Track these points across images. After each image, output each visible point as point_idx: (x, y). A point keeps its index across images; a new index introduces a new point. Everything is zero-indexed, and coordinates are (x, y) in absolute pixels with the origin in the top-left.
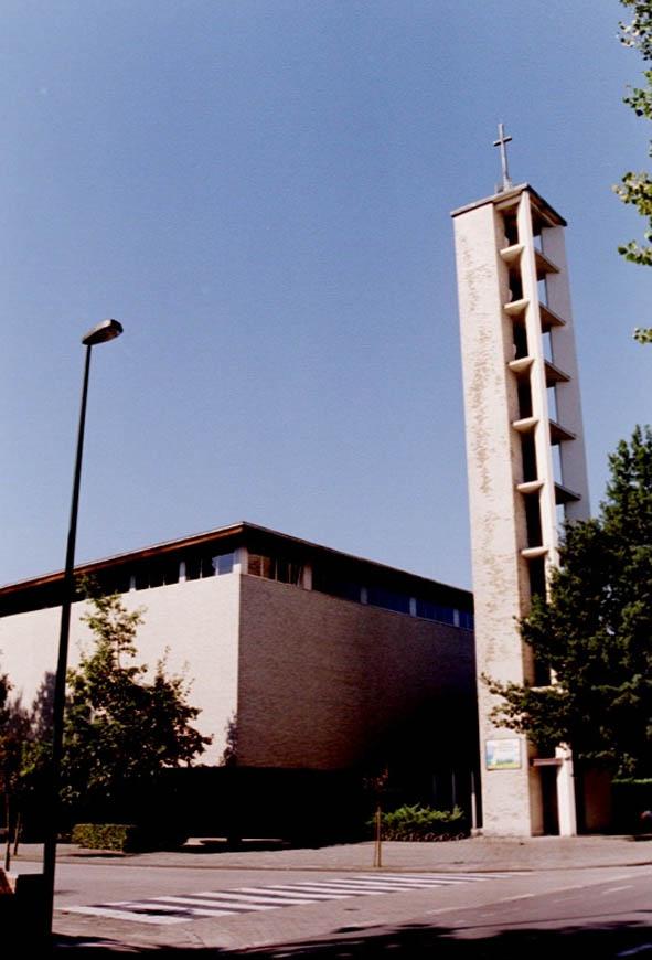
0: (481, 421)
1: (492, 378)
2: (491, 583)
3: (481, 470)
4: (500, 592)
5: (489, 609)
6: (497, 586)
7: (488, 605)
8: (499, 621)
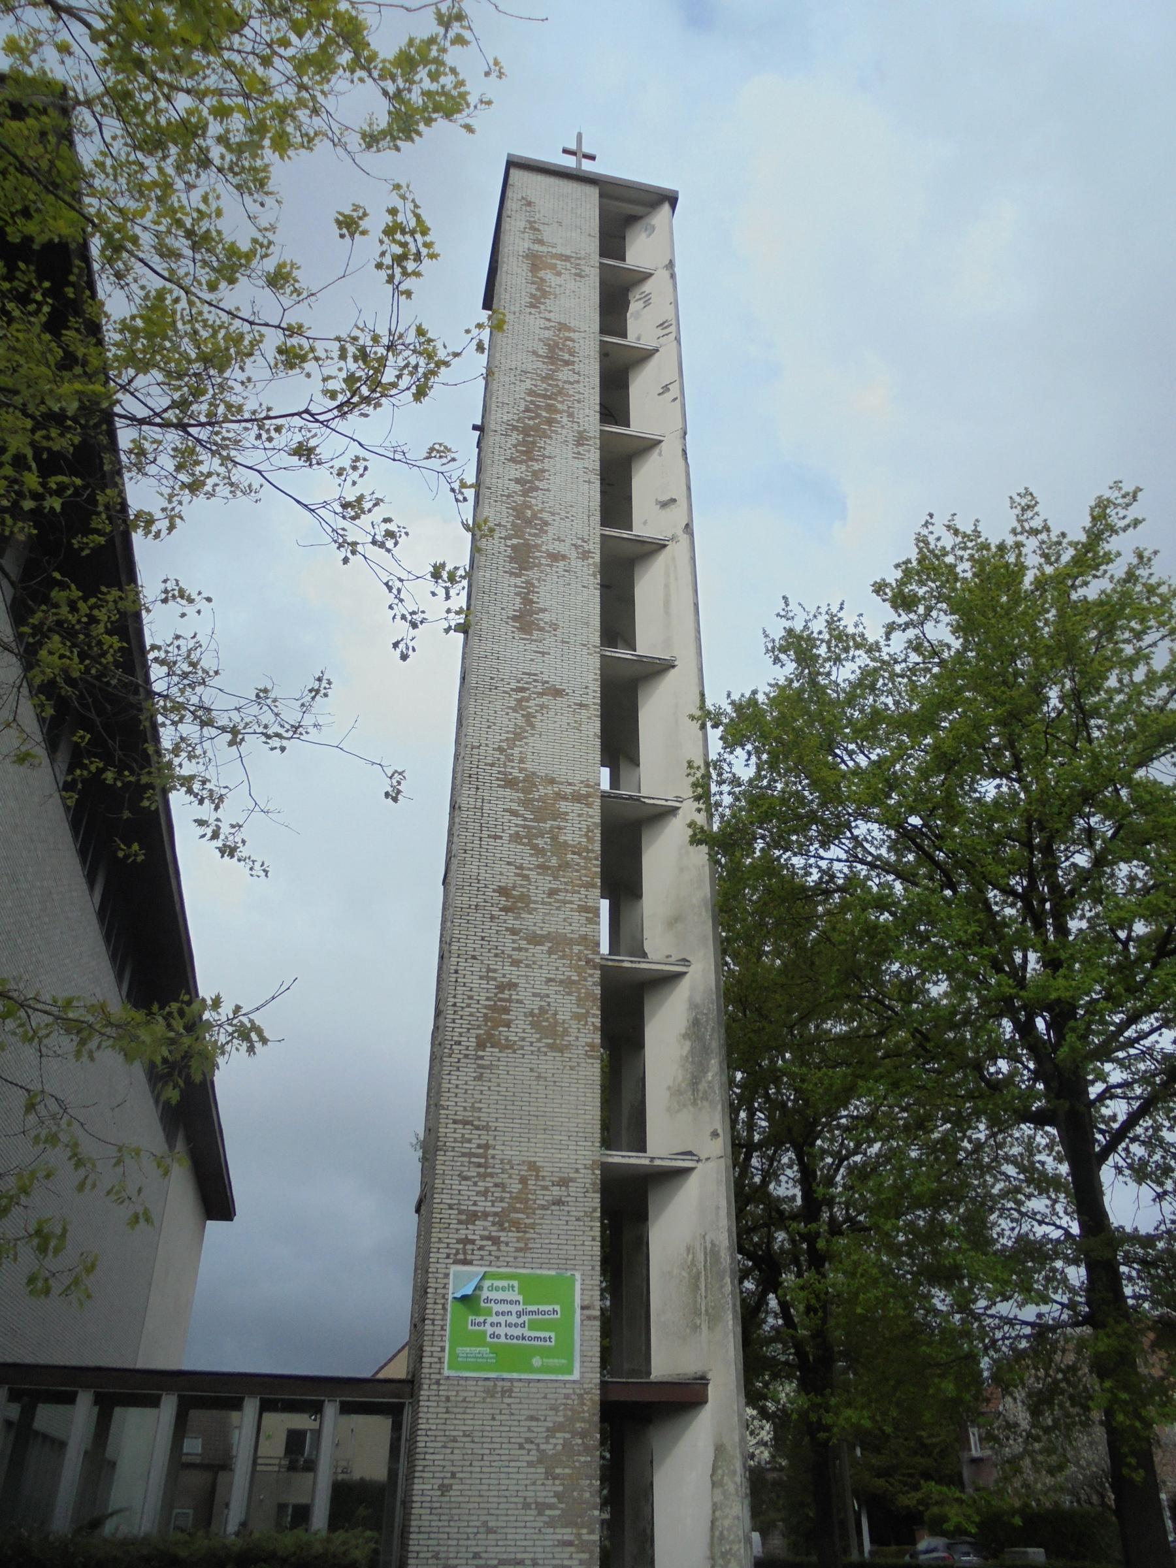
0: (525, 494)
1: (566, 430)
2: (516, 838)
3: (518, 581)
4: (543, 868)
5: (503, 901)
6: (538, 851)
7: (503, 891)
8: (535, 940)
